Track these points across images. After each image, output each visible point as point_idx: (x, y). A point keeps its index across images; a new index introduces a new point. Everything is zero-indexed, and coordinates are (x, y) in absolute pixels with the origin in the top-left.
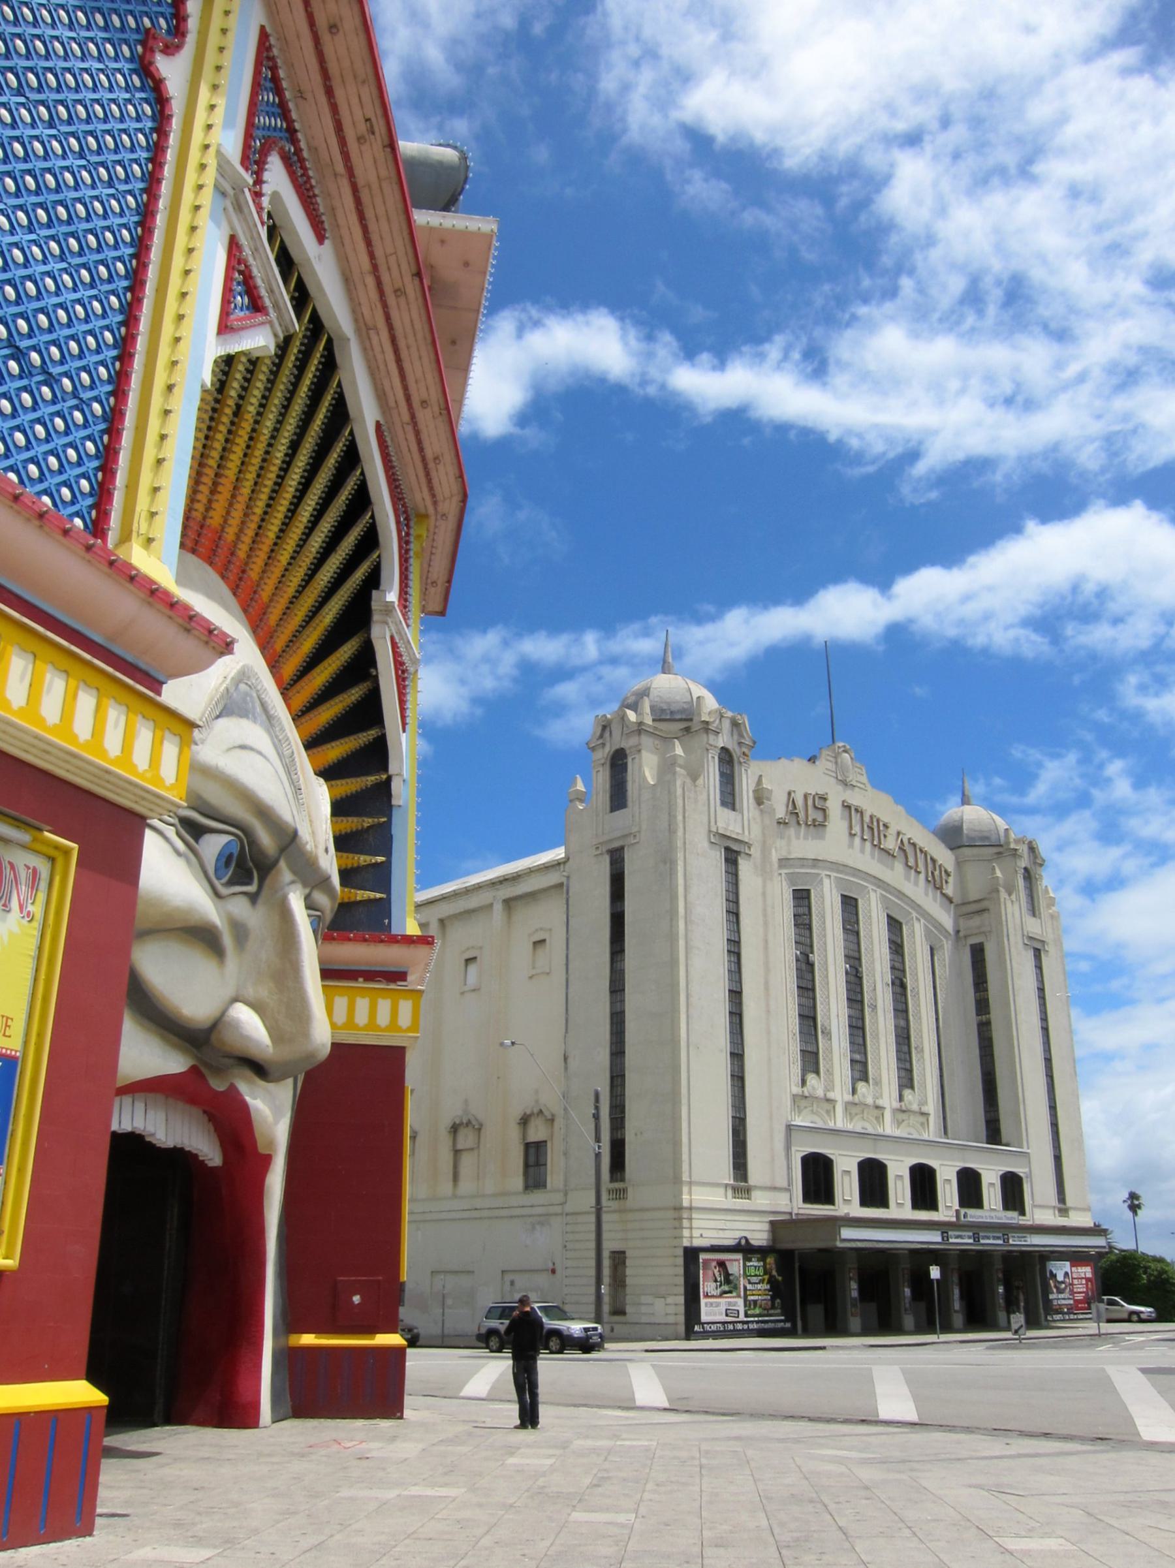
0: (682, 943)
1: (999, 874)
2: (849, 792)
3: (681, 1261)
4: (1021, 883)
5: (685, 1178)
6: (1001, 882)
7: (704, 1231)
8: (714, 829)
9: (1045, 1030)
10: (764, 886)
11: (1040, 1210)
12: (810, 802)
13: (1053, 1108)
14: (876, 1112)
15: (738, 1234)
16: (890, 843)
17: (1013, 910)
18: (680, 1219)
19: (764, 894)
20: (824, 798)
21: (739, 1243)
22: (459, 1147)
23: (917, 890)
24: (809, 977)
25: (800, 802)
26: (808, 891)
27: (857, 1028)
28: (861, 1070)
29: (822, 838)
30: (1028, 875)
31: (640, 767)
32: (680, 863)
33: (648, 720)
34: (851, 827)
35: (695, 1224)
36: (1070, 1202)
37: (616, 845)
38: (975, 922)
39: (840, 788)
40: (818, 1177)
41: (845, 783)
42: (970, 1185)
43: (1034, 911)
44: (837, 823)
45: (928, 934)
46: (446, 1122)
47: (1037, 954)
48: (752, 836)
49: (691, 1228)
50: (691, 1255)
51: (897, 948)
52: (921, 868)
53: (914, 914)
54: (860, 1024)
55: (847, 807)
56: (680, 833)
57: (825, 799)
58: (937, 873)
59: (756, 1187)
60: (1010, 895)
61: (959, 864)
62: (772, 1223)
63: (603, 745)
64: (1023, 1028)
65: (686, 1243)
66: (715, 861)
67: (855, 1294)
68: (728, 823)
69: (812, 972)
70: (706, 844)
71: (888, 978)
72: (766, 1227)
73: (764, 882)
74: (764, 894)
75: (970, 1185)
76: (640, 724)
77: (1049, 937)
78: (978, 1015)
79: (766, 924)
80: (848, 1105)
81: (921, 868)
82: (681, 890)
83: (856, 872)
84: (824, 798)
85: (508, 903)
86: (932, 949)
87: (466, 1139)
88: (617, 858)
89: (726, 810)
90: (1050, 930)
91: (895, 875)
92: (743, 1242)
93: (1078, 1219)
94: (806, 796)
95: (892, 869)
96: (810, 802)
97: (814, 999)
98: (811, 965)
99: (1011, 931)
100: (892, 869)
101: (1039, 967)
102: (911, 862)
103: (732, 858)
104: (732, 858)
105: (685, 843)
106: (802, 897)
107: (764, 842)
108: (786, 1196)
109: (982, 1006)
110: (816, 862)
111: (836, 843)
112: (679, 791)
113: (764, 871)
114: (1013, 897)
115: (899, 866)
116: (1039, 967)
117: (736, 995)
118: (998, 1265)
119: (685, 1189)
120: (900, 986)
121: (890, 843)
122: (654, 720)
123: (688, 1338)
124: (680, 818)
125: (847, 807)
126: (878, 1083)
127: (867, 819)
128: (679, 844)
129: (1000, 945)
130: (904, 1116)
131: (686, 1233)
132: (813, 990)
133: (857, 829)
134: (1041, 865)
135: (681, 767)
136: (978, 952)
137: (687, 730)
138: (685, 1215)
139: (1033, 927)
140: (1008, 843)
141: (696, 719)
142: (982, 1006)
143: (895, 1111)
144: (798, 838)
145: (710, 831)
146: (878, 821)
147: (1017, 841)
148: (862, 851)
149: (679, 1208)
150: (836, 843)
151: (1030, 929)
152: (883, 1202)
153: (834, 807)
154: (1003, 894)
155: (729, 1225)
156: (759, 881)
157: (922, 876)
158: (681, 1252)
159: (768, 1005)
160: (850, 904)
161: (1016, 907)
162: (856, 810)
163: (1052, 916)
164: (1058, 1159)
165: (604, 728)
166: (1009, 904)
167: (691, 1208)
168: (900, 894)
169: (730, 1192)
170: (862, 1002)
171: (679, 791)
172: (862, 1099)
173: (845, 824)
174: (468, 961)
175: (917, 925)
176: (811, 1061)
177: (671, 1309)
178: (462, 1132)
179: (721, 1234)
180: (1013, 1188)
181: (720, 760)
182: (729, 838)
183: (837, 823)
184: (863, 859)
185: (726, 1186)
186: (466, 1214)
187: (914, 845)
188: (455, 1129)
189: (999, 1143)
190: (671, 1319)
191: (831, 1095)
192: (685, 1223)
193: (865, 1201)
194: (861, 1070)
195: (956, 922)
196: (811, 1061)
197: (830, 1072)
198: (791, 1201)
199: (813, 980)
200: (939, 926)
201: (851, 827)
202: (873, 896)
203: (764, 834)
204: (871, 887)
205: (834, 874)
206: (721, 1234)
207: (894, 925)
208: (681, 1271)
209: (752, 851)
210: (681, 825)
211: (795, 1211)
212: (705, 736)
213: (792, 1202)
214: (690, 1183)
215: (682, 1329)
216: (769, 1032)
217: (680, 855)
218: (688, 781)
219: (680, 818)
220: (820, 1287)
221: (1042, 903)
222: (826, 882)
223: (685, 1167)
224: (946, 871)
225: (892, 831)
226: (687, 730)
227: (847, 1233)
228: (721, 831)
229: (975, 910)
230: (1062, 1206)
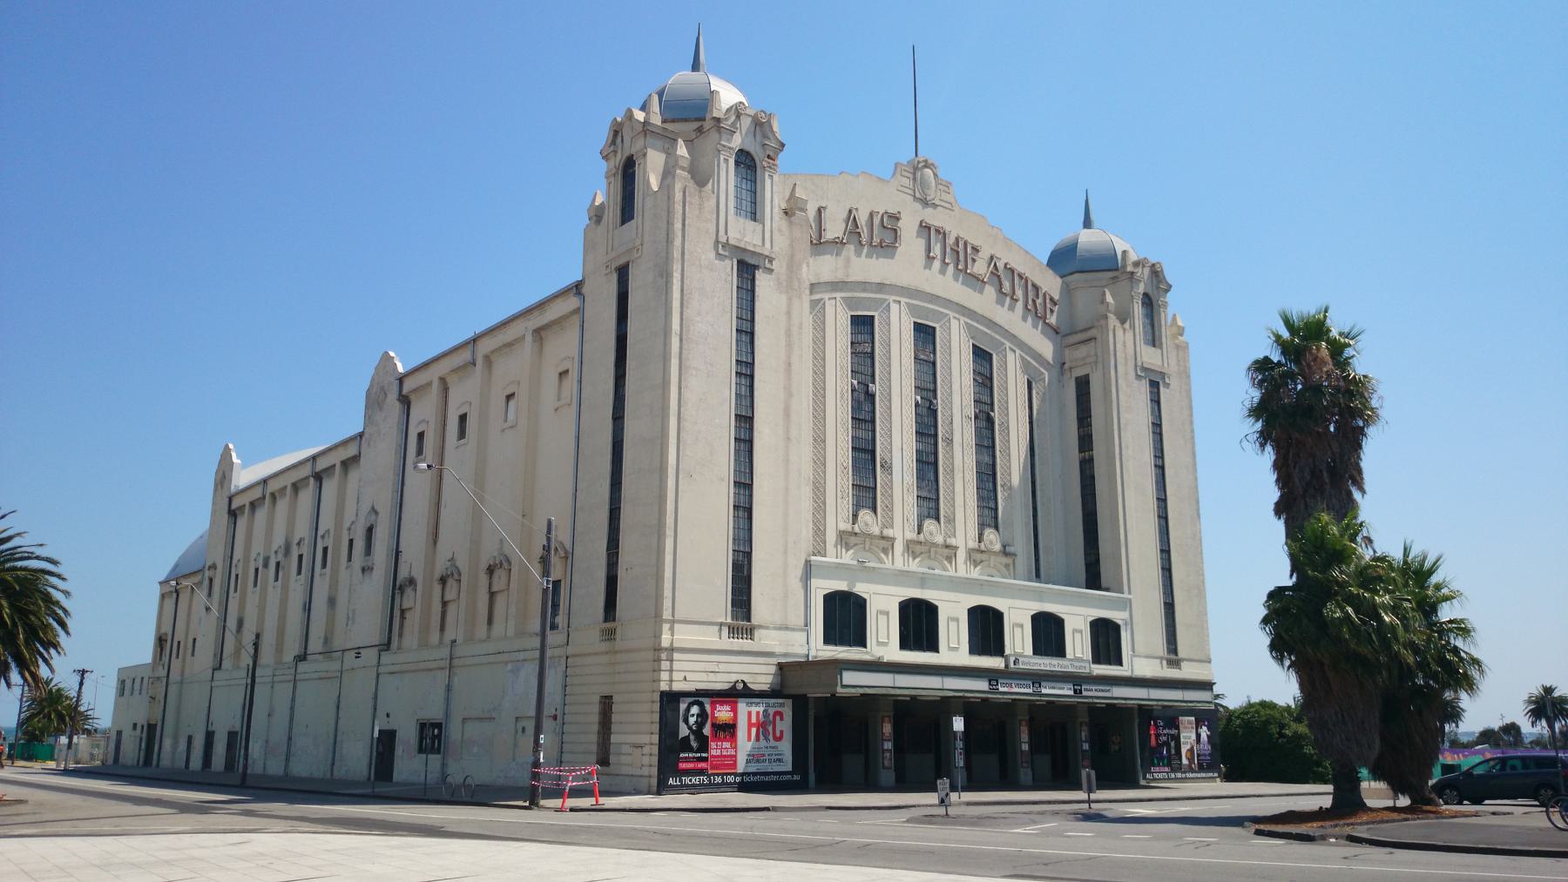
0: (674, 362)
1: (1109, 299)
2: (929, 210)
3: (657, 707)
4: (1138, 309)
5: (667, 615)
6: (1112, 308)
7: (686, 675)
8: (723, 239)
9: (1160, 469)
10: (789, 305)
11: (1142, 657)
12: (877, 221)
13: (1166, 552)
14: (883, 543)
15: (734, 678)
16: (980, 268)
17: (1125, 342)
18: (659, 660)
19: (789, 313)
20: (895, 218)
21: (734, 686)
22: (495, 589)
23: (1012, 319)
24: (867, 407)
25: (862, 219)
26: (872, 317)
27: (928, 465)
28: (930, 504)
29: (892, 257)
30: (1149, 302)
31: (645, 172)
32: (677, 276)
33: (656, 120)
34: (929, 250)
35: (676, 666)
36: (1182, 653)
37: (622, 261)
38: (1083, 351)
39: (918, 206)
40: (845, 618)
41: (925, 203)
42: (1048, 633)
43: (1154, 341)
44: (911, 244)
45: (1026, 366)
46: (484, 566)
47: (1155, 385)
48: (776, 249)
49: (671, 671)
50: (670, 699)
51: (984, 381)
52: (1019, 293)
53: (1008, 344)
54: (932, 459)
55: (925, 228)
56: (678, 242)
57: (898, 219)
58: (1039, 301)
59: (760, 627)
60: (1123, 322)
61: (1067, 290)
62: (781, 666)
63: (615, 152)
64: (1130, 465)
65: (664, 687)
66: (725, 275)
67: (1025, 747)
68: (744, 233)
69: (873, 404)
70: (712, 255)
71: (971, 411)
72: (773, 669)
73: (790, 299)
74: (789, 313)
75: (1048, 633)
76: (646, 123)
77: (1171, 367)
78: (1081, 451)
79: (789, 345)
80: (911, 548)
81: (1019, 293)
82: (676, 304)
83: (933, 298)
84: (895, 218)
85: (539, 332)
86: (1030, 383)
87: (499, 582)
88: (623, 273)
89: (742, 220)
90: (1173, 362)
91: (984, 301)
92: (740, 686)
93: (1188, 672)
94: (871, 215)
95: (981, 292)
96: (877, 221)
97: (874, 431)
98: (871, 397)
99: (1120, 360)
100: (981, 292)
101: (1156, 401)
102: (1007, 285)
103: (747, 269)
104: (747, 269)
105: (683, 254)
106: (863, 325)
107: (792, 256)
108: (801, 636)
109: (1086, 442)
110: (881, 287)
111: (908, 265)
112: (678, 196)
113: (789, 286)
114: (1127, 325)
115: (990, 291)
116: (1156, 401)
117: (745, 421)
118: (1084, 718)
119: (666, 627)
120: (985, 422)
121: (980, 268)
122: (664, 121)
123: (659, 793)
124: (678, 225)
125: (925, 228)
126: (951, 520)
127: (951, 241)
128: (676, 254)
129: (1106, 376)
130: (984, 556)
131: (664, 676)
132: (873, 421)
133: (937, 250)
134: (1167, 291)
135: (683, 169)
136: (1083, 385)
137: (700, 130)
138: (664, 656)
139: (1150, 357)
140: (1124, 266)
141: (708, 117)
142: (1086, 442)
143: (970, 552)
144: (859, 254)
145: (717, 242)
146: (966, 244)
147: (1136, 264)
148: (943, 272)
149: (658, 649)
150: (908, 265)
151: (1145, 359)
152: (933, 646)
153: (908, 227)
154: (1113, 320)
155: (722, 667)
156: (784, 298)
157: (1020, 305)
158: (657, 697)
159: (787, 430)
160: (925, 334)
161: (1129, 335)
162: (938, 231)
163: (1178, 347)
164: (1169, 607)
165: (616, 133)
166: (1119, 333)
167: (672, 649)
168: (991, 324)
169: (725, 631)
170: (936, 435)
171: (678, 196)
172: (929, 537)
173: (922, 243)
174: (509, 397)
175: (1010, 356)
176: (866, 494)
177: (646, 760)
178: (498, 572)
179: (712, 677)
180: (1106, 639)
181: (737, 163)
182: (745, 250)
183: (911, 244)
184: (946, 285)
185: (721, 624)
186: (491, 659)
187: (1012, 271)
188: (491, 571)
189: (1099, 588)
190: (645, 771)
191: (889, 532)
192: (665, 665)
193: (975, 649)
194: (930, 504)
195: (1059, 351)
196: (866, 494)
197: (889, 508)
198: (809, 642)
199: (874, 412)
200: (1038, 357)
201: (929, 250)
202: (954, 323)
203: (791, 246)
204: (952, 314)
205: (903, 300)
206: (712, 677)
207: (981, 356)
208: (656, 717)
209: (775, 265)
210: (679, 234)
211: (813, 653)
212: (716, 136)
213: (809, 642)
214: (673, 622)
215: (654, 782)
216: (787, 461)
217: (677, 267)
218: (691, 185)
219: (678, 225)
220: (842, 740)
221: (1166, 333)
222: (894, 308)
223: (667, 603)
224: (1052, 299)
225: (984, 254)
226: (700, 130)
227: (850, 678)
228: (732, 242)
229: (1078, 334)
230: (1173, 657)
